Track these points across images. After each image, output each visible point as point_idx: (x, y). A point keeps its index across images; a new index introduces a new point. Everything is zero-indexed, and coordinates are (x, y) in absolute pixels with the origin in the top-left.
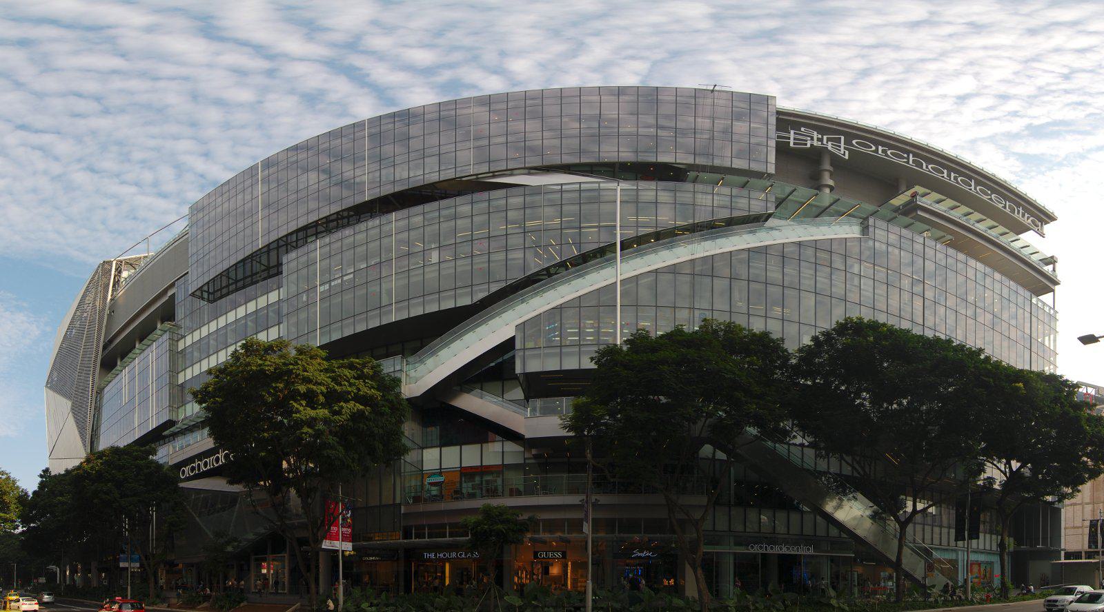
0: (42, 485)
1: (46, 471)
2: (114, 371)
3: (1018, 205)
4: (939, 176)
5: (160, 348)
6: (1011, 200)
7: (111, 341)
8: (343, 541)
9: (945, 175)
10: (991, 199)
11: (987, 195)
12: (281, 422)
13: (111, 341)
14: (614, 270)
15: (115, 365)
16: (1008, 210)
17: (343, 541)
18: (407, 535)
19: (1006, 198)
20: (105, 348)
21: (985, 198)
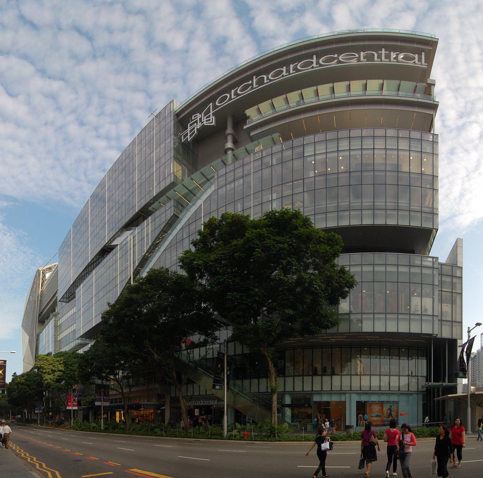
0: (13, 380)
1: (15, 373)
2: (44, 325)
3: (378, 49)
4: (410, 63)
5: (98, 303)
6: (363, 49)
7: (42, 313)
8: (103, 401)
9: (416, 60)
10: (340, 62)
11: (334, 59)
12: (214, 311)
13: (42, 313)
14: (204, 221)
15: (44, 322)
16: (363, 61)
17: (103, 401)
18: (112, 402)
19: (358, 50)
20: (40, 315)
21: (333, 64)
